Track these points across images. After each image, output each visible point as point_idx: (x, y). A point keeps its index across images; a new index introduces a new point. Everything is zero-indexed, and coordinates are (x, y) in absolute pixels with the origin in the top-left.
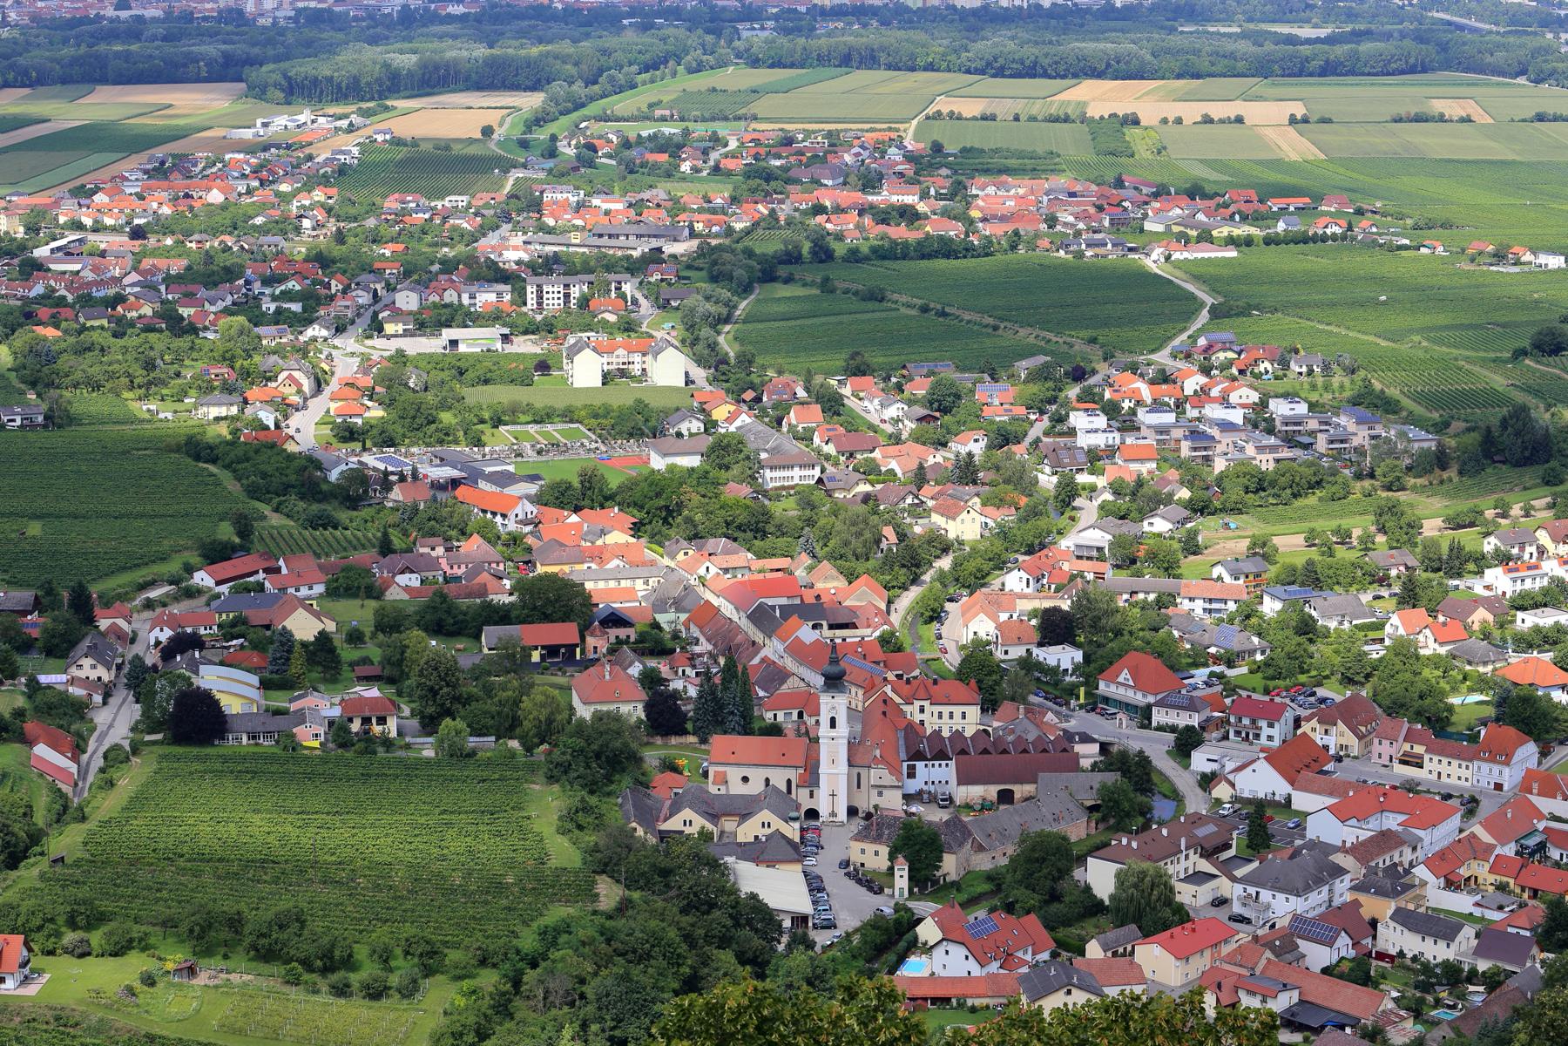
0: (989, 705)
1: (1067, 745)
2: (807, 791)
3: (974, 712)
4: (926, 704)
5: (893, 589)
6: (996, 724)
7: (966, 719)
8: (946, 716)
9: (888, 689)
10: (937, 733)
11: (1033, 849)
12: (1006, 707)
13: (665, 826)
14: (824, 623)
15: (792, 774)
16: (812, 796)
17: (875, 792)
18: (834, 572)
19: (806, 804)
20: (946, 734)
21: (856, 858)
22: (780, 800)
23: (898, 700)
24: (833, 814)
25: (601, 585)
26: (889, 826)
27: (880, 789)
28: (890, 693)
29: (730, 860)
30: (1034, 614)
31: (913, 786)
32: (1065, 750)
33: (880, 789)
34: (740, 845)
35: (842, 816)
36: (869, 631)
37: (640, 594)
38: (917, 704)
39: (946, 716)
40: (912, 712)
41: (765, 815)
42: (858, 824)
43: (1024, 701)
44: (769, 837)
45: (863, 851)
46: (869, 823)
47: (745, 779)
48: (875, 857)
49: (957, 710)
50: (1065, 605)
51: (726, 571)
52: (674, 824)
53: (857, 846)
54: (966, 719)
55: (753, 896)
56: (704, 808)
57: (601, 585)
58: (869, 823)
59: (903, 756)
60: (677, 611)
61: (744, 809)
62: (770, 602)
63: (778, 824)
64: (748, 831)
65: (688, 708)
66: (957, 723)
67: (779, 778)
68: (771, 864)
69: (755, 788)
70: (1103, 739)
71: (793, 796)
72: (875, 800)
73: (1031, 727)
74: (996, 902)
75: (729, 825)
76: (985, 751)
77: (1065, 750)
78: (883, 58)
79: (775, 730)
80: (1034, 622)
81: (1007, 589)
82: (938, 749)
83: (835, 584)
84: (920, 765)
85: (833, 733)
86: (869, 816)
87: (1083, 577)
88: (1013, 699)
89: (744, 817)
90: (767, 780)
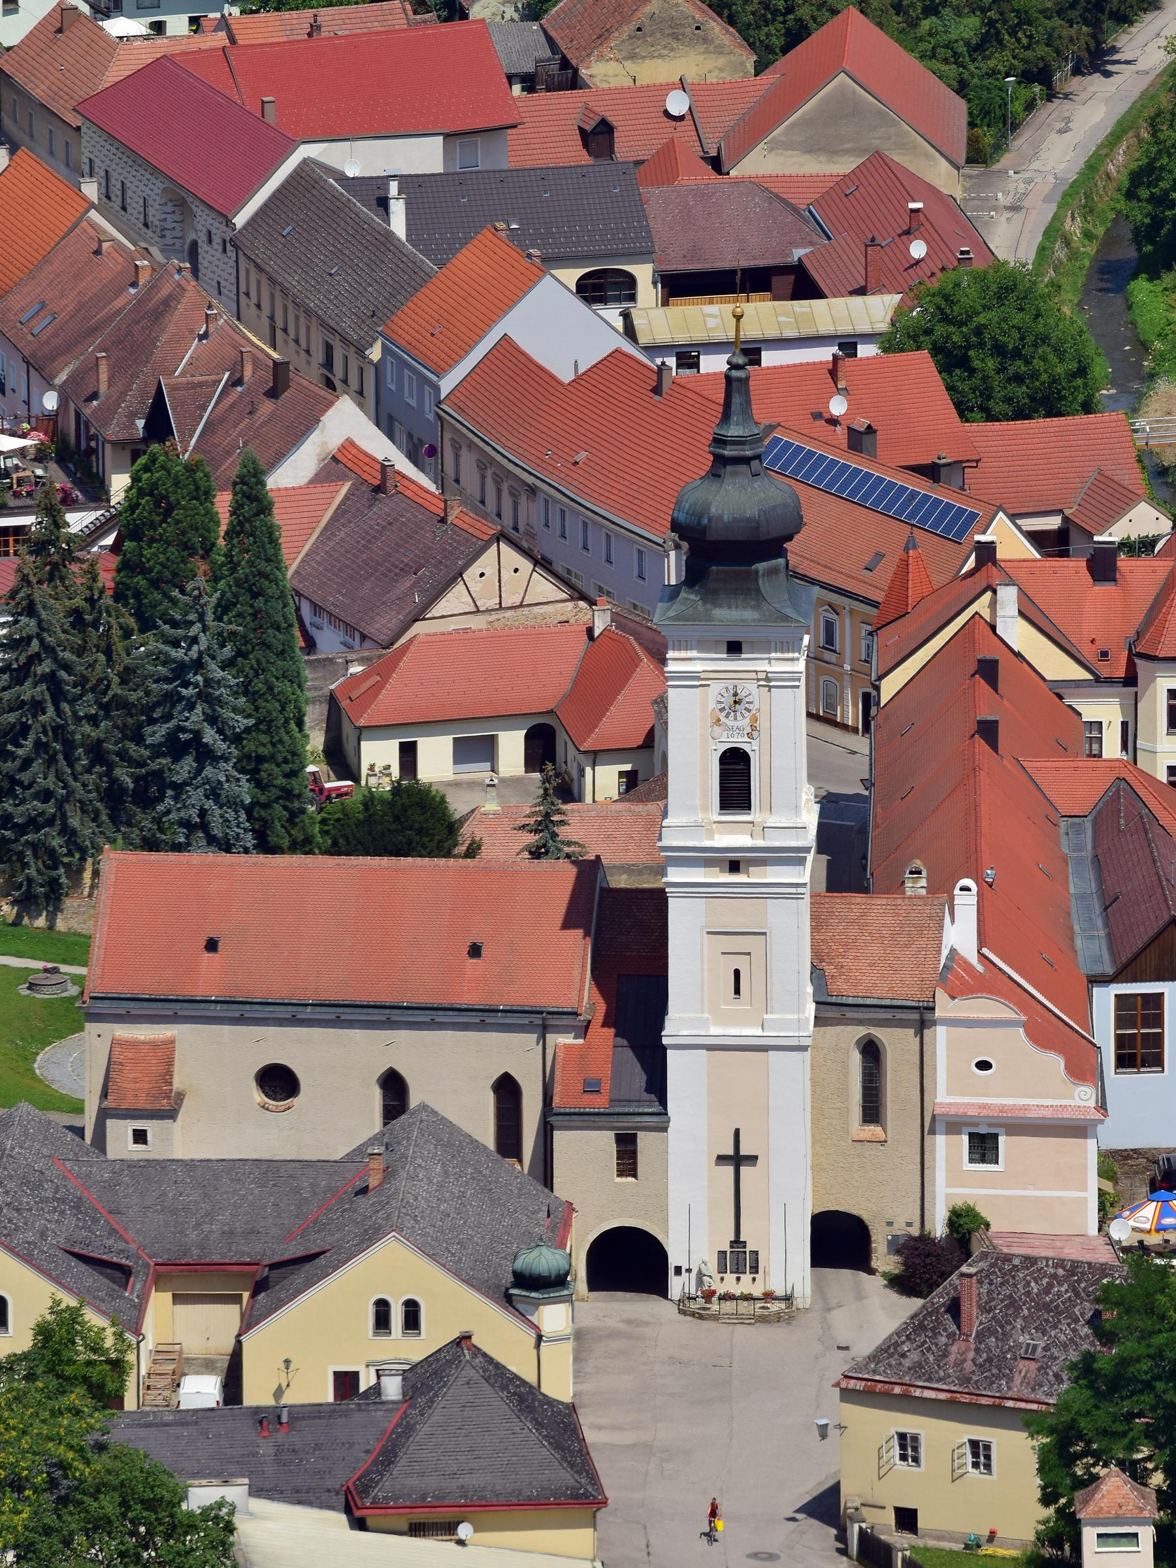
16: (628, 1162)
17: (948, 1151)
23: (1055, 665)
24: (739, 1257)
26: (1047, 1313)
28: (1017, 633)
35: (788, 1262)
44: (424, 1379)
56: (65, 1229)
59: (1091, 947)
62: (356, 159)
63: (457, 1309)
64: (308, 1347)
67: (455, 1077)
68: (431, 1522)
69: (334, 1119)
70: (889, 1139)
72: (955, 1180)
79: (413, 824)
83: (691, 64)
86: (927, 1265)
89: (266, 1282)
90: (394, 1087)
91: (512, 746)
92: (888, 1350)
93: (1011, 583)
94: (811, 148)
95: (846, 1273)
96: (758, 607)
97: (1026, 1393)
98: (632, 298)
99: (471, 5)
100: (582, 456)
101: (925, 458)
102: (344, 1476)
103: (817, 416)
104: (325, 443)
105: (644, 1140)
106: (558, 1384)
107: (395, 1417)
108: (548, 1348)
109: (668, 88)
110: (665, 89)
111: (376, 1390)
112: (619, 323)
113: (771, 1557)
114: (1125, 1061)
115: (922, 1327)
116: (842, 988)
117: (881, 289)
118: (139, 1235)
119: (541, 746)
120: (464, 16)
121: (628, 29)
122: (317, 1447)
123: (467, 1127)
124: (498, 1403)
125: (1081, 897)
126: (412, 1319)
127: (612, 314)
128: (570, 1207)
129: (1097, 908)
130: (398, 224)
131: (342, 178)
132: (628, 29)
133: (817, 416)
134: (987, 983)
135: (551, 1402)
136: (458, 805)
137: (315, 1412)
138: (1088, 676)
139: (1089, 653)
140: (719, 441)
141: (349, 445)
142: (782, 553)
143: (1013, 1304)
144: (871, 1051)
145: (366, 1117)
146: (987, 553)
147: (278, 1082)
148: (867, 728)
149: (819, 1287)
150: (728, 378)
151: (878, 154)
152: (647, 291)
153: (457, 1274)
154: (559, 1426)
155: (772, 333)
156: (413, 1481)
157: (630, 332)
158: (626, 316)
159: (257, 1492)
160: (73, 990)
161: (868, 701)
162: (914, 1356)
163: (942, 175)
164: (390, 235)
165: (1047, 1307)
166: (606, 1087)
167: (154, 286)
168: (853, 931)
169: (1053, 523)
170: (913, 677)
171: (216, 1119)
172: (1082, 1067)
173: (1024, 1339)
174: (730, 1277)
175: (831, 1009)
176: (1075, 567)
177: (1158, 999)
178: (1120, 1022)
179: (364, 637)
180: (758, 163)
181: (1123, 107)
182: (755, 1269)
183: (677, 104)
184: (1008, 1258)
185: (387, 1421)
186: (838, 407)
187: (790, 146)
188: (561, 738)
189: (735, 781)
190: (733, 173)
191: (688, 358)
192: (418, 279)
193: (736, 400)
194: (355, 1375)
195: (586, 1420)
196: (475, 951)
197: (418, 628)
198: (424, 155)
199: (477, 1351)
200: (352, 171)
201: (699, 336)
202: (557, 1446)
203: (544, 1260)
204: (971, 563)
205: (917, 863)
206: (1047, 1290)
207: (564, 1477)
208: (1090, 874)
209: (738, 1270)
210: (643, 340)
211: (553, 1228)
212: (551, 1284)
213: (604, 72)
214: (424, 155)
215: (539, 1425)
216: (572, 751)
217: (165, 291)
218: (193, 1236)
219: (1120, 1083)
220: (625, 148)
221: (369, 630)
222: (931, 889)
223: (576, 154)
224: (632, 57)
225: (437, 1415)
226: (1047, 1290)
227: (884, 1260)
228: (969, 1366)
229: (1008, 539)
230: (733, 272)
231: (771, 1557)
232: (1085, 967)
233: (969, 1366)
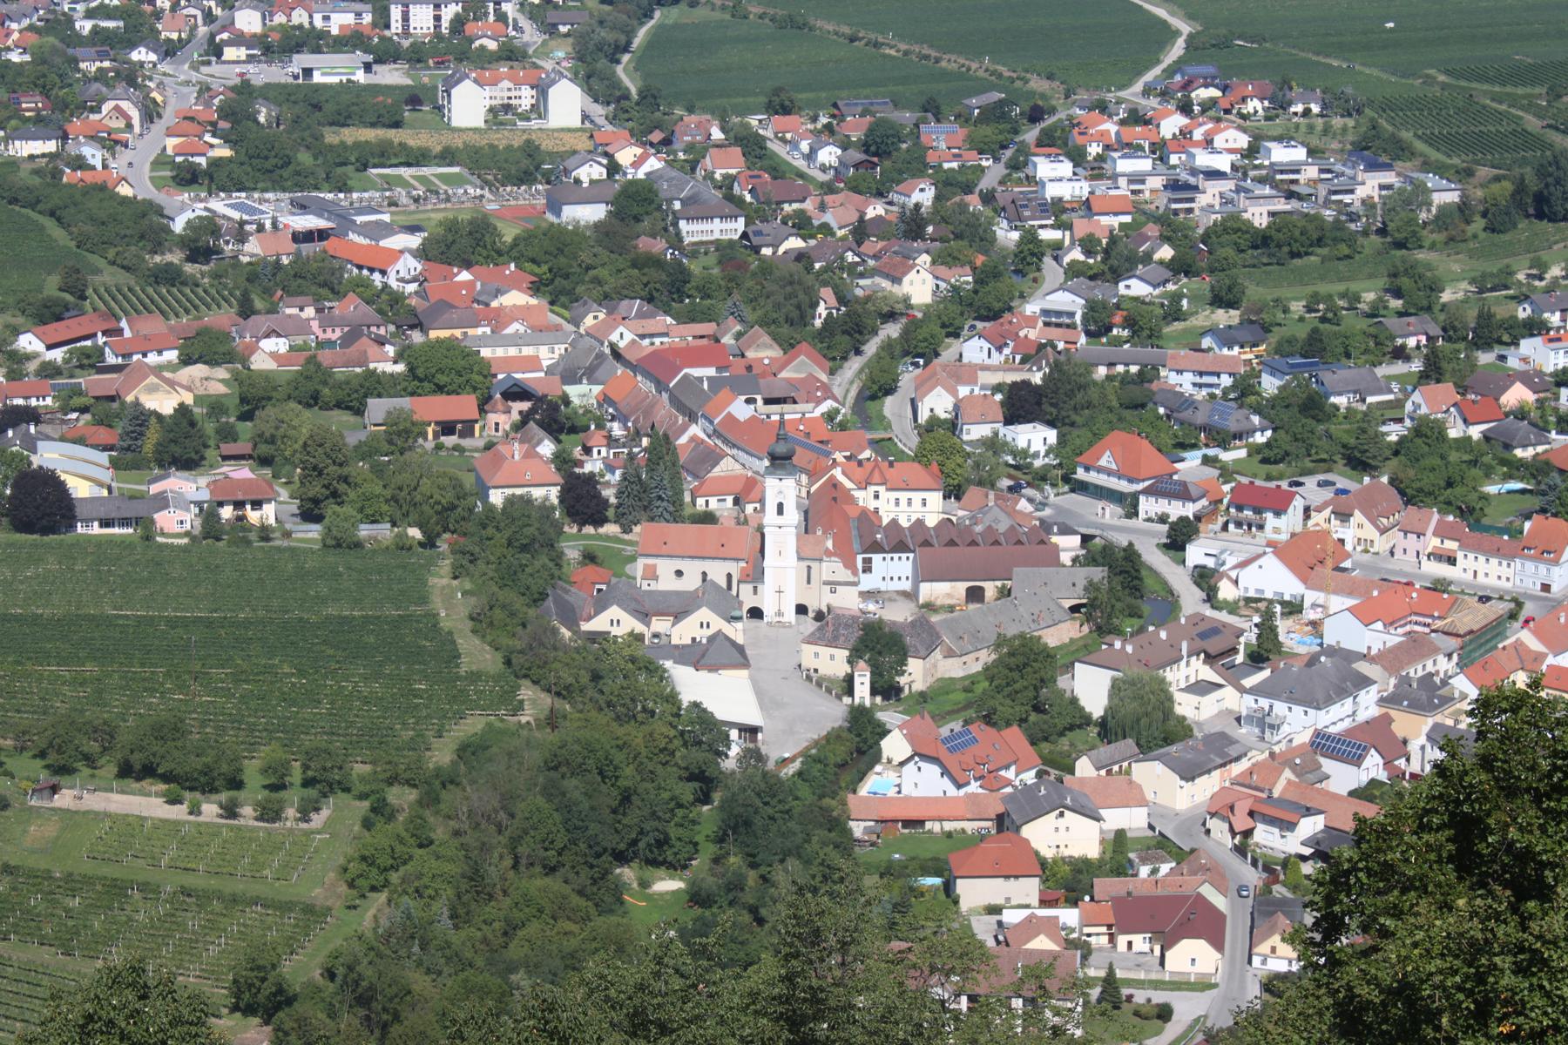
23: (848, 484)
24: (779, 613)
35: (790, 615)
44: (711, 639)
56: (633, 605)
59: (856, 546)
63: (718, 624)
64: (685, 632)
68: (713, 668)
69: (691, 582)
79: (708, 518)
86: (819, 616)
89: (678, 616)
90: (704, 574)
91: (730, 499)
106: (740, 641)
108: (736, 632)
130: (706, 386)
136: (718, 514)
145: (698, 582)
147: (679, 573)
152: (760, 402)
154: (740, 649)
163: (824, 377)
170: (692, 557)
171: (666, 582)
172: (855, 573)
189: (780, 509)
192: (709, 398)
198: (711, 372)
203: (736, 613)
212: (739, 619)
213: (750, 354)
214: (711, 372)
229: (839, 456)
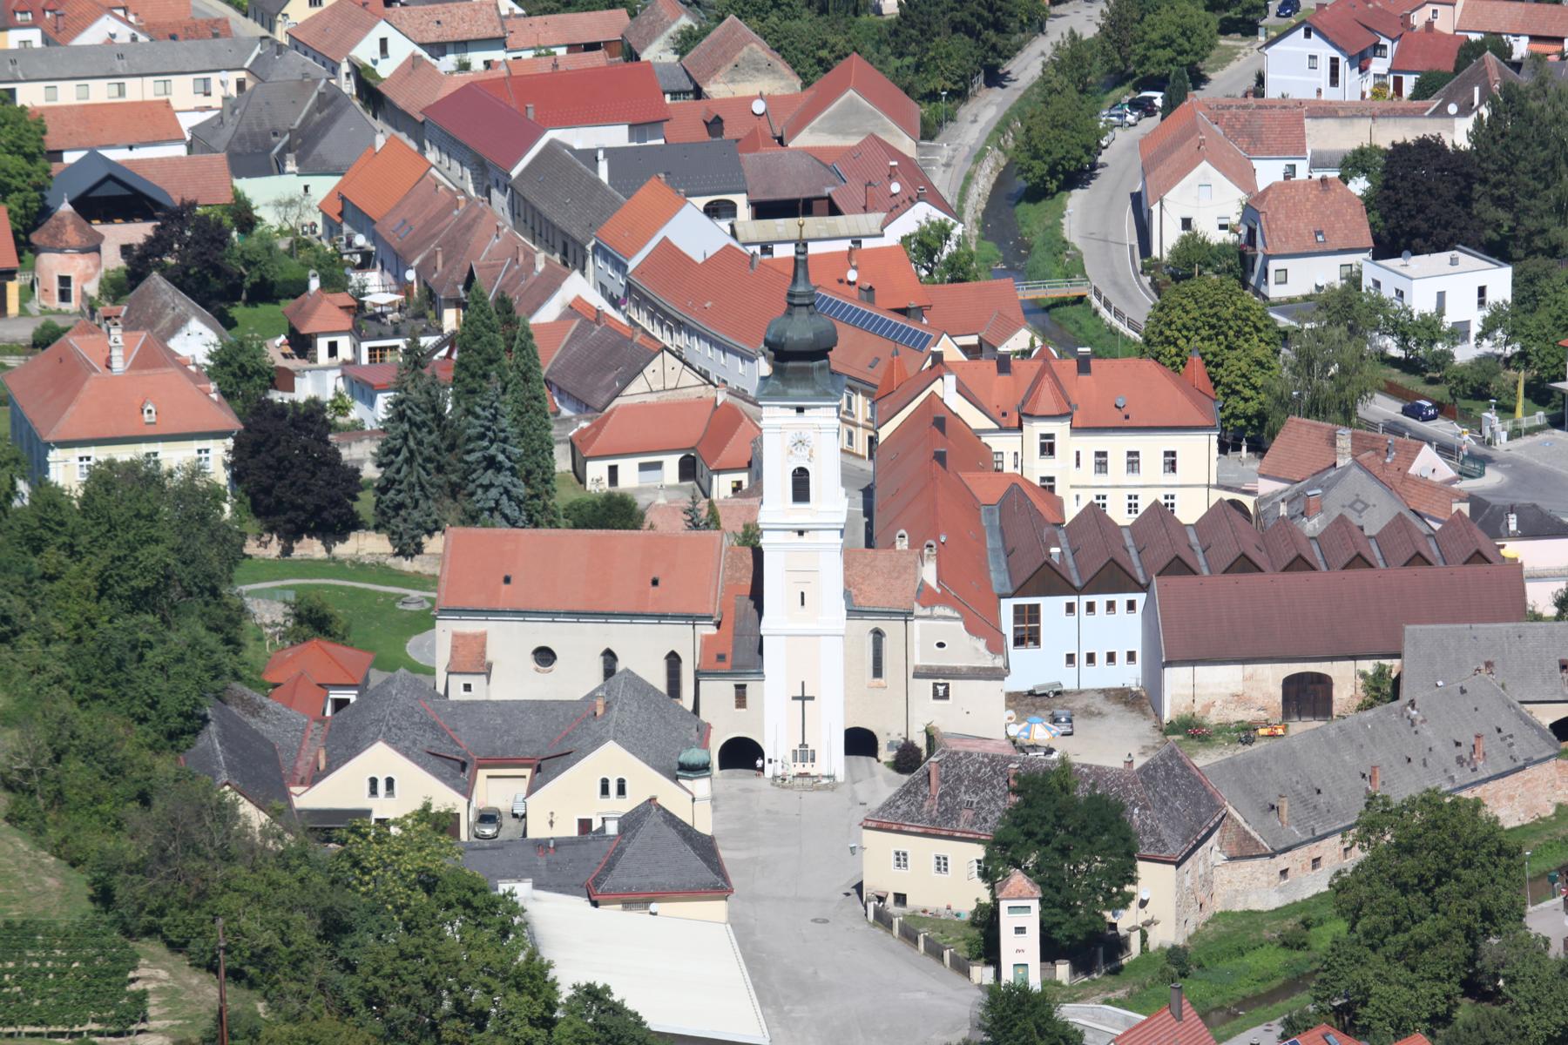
0: (1245, 434)
1: (1483, 542)
2: (727, 687)
3: (1198, 451)
4: (1060, 429)
5: (935, 104)
6: (1266, 487)
7: (1184, 474)
8: (1117, 462)
9: (946, 388)
10: (1095, 513)
11: (1405, 849)
12: (1297, 436)
13: (307, 799)
14: (741, 200)
15: (686, 640)
18: (758, 49)
19: (724, 724)
20: (1120, 515)
21: (881, 877)
22: (651, 716)
23: (975, 419)
24: (804, 753)
25: (68, 94)
26: (978, 783)
27: (941, 679)
28: (956, 403)
29: (523, 890)
30: (1355, 163)
31: (1032, 668)
32: (1479, 557)
33: (941, 679)
34: (541, 844)
35: (832, 758)
36: (873, 220)
37: (187, 122)
38: (1034, 430)
39: (1117, 462)
40: (1015, 452)
41: (611, 759)
42: (880, 782)
43: (1348, 415)
44: (630, 823)
45: (901, 858)
46: (921, 779)
47: (545, 656)
48: (944, 876)
49: (1152, 447)
50: (1458, 134)
51: (438, 49)
52: (339, 790)
53: (881, 845)
54: (1184, 474)
55: (593, 995)
56: (428, 740)
57: (68, 94)
58: (921, 779)
59: (998, 578)
60: (309, 167)
61: (546, 745)
62: (579, 138)
63: (646, 783)
64: (561, 806)
65: (361, 455)
66: (1151, 485)
67: (644, 650)
68: (637, 899)
69: (576, 678)
71: (687, 702)
73: (1373, 493)
74: (1304, 1002)
75: (497, 790)
76: (1244, 564)
77: (1479, 557)
78: (1341, 113)
79: (617, 512)
80: (1359, 185)
81: (1272, 92)
82: (1104, 561)
84: (1051, 607)
85: (801, 514)
86: (907, 759)
87: (1504, 52)
88: (1315, 409)
89: (544, 767)
90: (609, 656)
91: (672, 463)
92: (890, 804)
93: (951, 373)
94: (834, 131)
95: (863, 758)
96: (813, 388)
97: (968, 828)
98: (735, 215)
99: (643, 49)
100: (708, 305)
101: (902, 306)
102: (587, 877)
103: (841, 281)
104: (784, 331)
105: (752, 687)
107: (614, 845)
108: (695, 803)
109: (753, 98)
110: (752, 99)
111: (603, 829)
112: (728, 230)
113: (826, 921)
114: (1019, 642)
115: (908, 792)
116: (862, 603)
117: (875, 210)
118: (467, 741)
119: (688, 469)
120: (638, 59)
121: (730, 66)
122: (571, 861)
123: (651, 681)
124: (671, 834)
125: (994, 550)
126: (621, 790)
127: (724, 224)
128: (709, 726)
129: (1003, 557)
131: (572, 150)
132: (730, 66)
133: (841, 281)
134: (942, 599)
135: (702, 836)
136: (642, 501)
137: (569, 841)
138: (995, 426)
139: (996, 413)
140: (791, 295)
141: (578, 299)
142: (827, 357)
143: (959, 779)
144: (878, 634)
145: (595, 678)
146: (938, 357)
148: (871, 456)
149: (849, 769)
150: (796, 260)
151: (873, 135)
152: (744, 212)
153: (647, 762)
154: (705, 847)
155: (814, 235)
156: (625, 880)
157: (734, 234)
158: (732, 226)
159: (537, 886)
160: (428, 605)
161: (872, 440)
162: (904, 808)
163: (907, 145)
164: (599, 181)
165: (979, 780)
166: (729, 658)
167: (467, 212)
168: (868, 570)
169: (973, 340)
171: (512, 680)
172: (996, 646)
173: (967, 798)
174: (799, 765)
175: (854, 612)
176: (988, 366)
177: (1037, 607)
178: (1017, 619)
179: (587, 406)
180: (804, 139)
181: (1006, 108)
182: (813, 760)
183: (759, 107)
184: (956, 753)
185: (609, 847)
186: (852, 275)
187: (822, 130)
188: (699, 462)
189: (801, 486)
190: (790, 145)
191: (766, 249)
192: (615, 205)
193: (801, 273)
194: (590, 821)
195: (719, 843)
196: (655, 583)
197: (618, 401)
198: (617, 136)
199: (660, 807)
200: (577, 146)
201: (773, 237)
202: (705, 860)
203: (693, 756)
204: (929, 363)
205: (902, 532)
206: (979, 770)
207: (711, 877)
208: (998, 537)
209: (804, 760)
210: (742, 238)
211: (700, 737)
212: (701, 769)
213: (717, 89)
214: (617, 136)
215: (694, 848)
216: (705, 470)
217: (473, 215)
218: (499, 743)
219: (1018, 656)
220: (729, 133)
221: (591, 403)
222: (911, 546)
223: (702, 134)
224: (733, 81)
225: (637, 842)
226: (979, 770)
227: (886, 754)
228: (935, 813)
229: (949, 348)
230: (796, 201)
231: (826, 921)
232: (996, 589)
233: (935, 813)
